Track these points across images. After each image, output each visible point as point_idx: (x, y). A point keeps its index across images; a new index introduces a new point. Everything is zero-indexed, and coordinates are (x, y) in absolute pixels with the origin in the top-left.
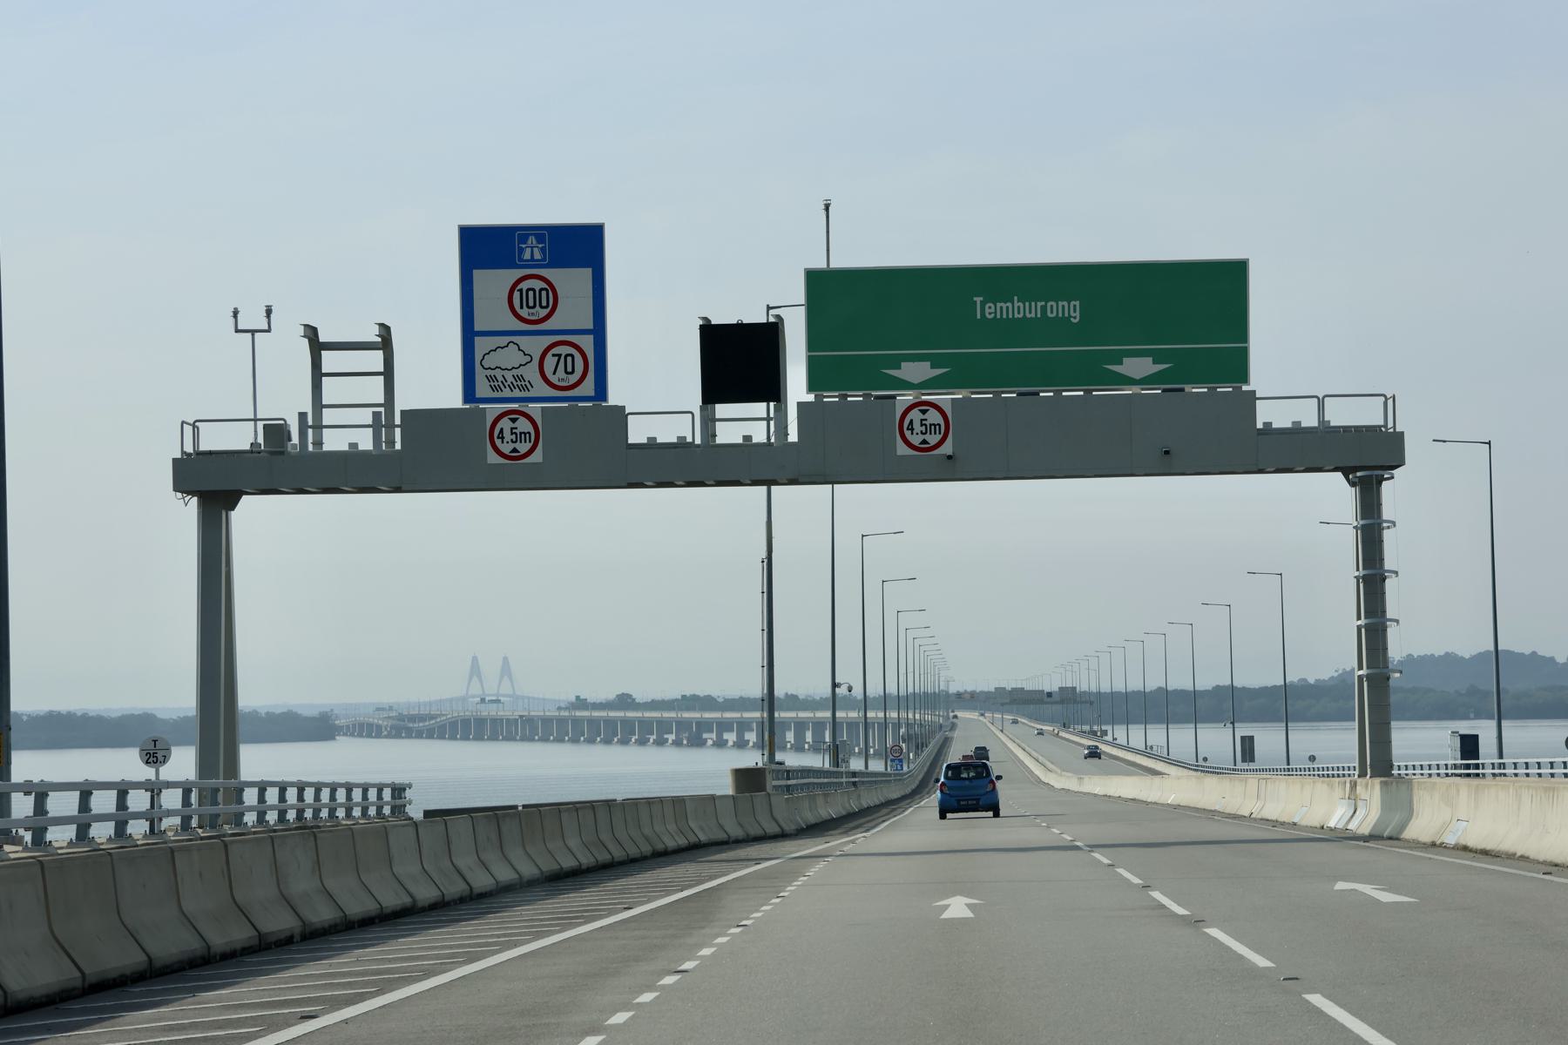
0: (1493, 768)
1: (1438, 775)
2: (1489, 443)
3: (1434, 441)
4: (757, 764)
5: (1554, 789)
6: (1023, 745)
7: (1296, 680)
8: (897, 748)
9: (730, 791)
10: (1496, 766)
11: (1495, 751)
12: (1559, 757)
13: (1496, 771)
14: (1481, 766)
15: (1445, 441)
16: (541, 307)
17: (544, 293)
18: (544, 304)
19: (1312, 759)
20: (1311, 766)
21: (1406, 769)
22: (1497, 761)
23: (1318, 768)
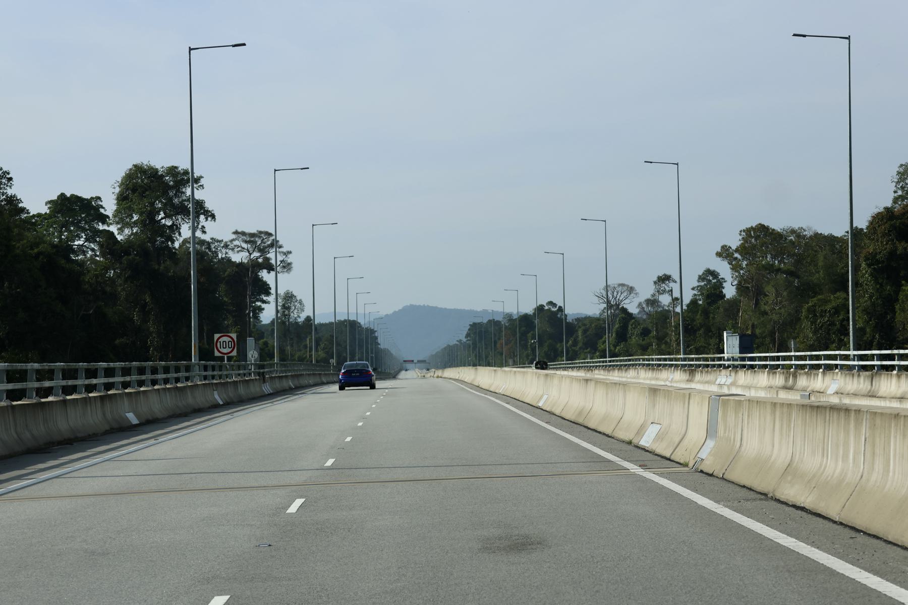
16: (229, 348)
17: (230, 343)
18: (230, 346)
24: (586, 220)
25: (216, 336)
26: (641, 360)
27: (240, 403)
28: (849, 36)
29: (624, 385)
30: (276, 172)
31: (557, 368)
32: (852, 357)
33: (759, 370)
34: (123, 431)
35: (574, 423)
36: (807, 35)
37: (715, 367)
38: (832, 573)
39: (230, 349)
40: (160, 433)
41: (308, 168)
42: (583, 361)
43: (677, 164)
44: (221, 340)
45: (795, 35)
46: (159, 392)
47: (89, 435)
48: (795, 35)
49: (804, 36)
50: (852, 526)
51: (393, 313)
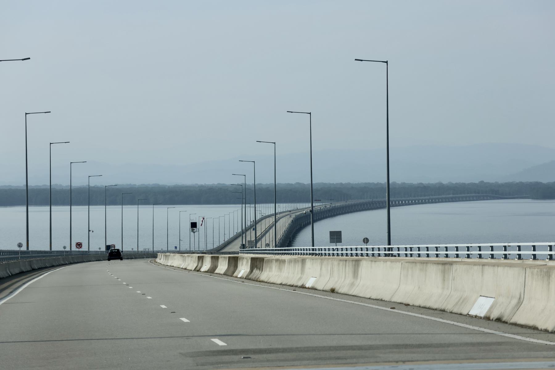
0: (385, 251)
1: (367, 255)
2: (310, 113)
3: (287, 112)
4: (65, 248)
5: (452, 264)
6: (398, 335)
7: (315, 183)
8: (113, 246)
9: (105, 250)
10: (387, 249)
11: (311, 244)
12: (415, 244)
13: (387, 252)
14: (315, 250)
15: (292, 112)
19: (366, 241)
20: (335, 247)
21: (329, 251)
22: (387, 246)
23: (301, 249)
49: (362, 60)
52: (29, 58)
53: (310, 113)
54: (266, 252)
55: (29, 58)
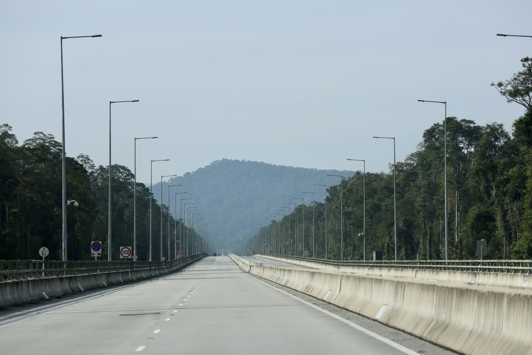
17: (128, 251)
18: (128, 253)
24: (350, 160)
25: (121, 248)
26: (418, 264)
27: (15, 308)
28: (446, 102)
29: (379, 281)
30: (63, 40)
31: (433, 268)
32: (446, 263)
33: (457, 271)
34: (18, 306)
35: (295, 290)
36: (507, 35)
37: (455, 269)
38: (134, 225)
39: (128, 255)
40: (19, 314)
41: (101, 36)
42: (400, 261)
43: (445, 103)
44: (124, 250)
45: (498, 35)
46: (137, 272)
47: (24, 302)
48: (418, 101)
49: (505, 36)
50: (431, 341)
51: (197, 171)
52: (138, 101)
53: (394, 138)
54: (348, 264)
55: (101, 36)
